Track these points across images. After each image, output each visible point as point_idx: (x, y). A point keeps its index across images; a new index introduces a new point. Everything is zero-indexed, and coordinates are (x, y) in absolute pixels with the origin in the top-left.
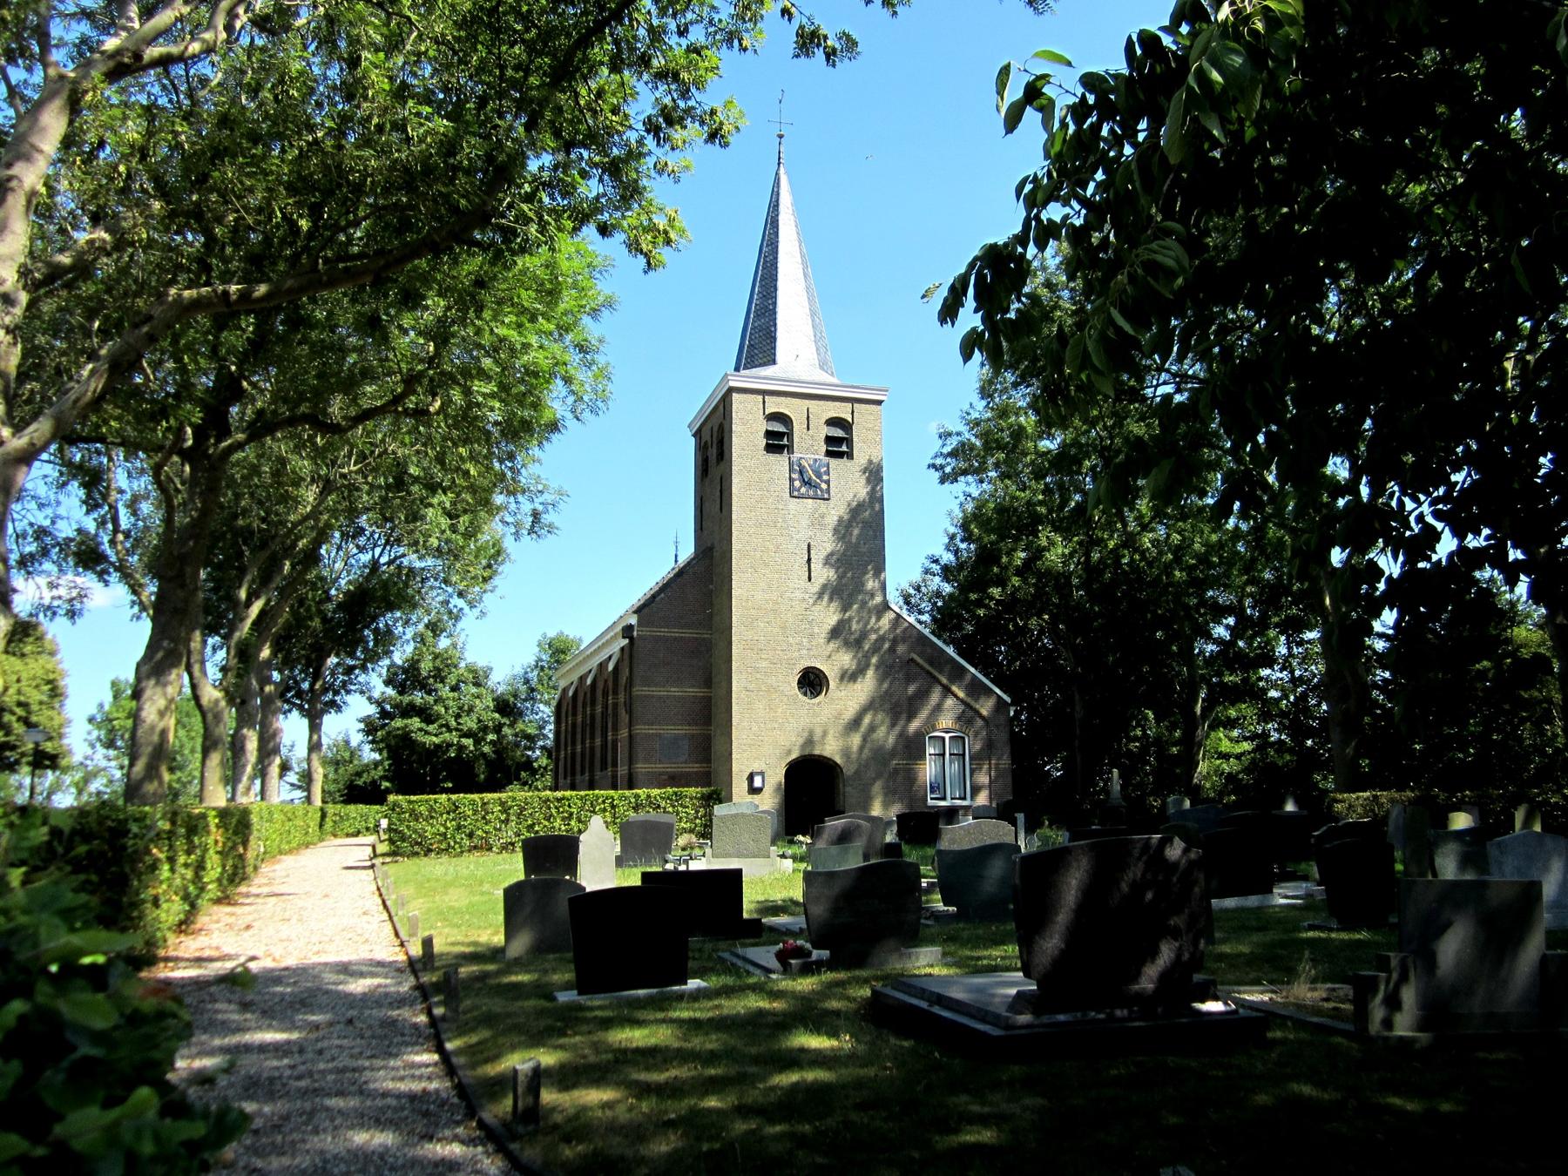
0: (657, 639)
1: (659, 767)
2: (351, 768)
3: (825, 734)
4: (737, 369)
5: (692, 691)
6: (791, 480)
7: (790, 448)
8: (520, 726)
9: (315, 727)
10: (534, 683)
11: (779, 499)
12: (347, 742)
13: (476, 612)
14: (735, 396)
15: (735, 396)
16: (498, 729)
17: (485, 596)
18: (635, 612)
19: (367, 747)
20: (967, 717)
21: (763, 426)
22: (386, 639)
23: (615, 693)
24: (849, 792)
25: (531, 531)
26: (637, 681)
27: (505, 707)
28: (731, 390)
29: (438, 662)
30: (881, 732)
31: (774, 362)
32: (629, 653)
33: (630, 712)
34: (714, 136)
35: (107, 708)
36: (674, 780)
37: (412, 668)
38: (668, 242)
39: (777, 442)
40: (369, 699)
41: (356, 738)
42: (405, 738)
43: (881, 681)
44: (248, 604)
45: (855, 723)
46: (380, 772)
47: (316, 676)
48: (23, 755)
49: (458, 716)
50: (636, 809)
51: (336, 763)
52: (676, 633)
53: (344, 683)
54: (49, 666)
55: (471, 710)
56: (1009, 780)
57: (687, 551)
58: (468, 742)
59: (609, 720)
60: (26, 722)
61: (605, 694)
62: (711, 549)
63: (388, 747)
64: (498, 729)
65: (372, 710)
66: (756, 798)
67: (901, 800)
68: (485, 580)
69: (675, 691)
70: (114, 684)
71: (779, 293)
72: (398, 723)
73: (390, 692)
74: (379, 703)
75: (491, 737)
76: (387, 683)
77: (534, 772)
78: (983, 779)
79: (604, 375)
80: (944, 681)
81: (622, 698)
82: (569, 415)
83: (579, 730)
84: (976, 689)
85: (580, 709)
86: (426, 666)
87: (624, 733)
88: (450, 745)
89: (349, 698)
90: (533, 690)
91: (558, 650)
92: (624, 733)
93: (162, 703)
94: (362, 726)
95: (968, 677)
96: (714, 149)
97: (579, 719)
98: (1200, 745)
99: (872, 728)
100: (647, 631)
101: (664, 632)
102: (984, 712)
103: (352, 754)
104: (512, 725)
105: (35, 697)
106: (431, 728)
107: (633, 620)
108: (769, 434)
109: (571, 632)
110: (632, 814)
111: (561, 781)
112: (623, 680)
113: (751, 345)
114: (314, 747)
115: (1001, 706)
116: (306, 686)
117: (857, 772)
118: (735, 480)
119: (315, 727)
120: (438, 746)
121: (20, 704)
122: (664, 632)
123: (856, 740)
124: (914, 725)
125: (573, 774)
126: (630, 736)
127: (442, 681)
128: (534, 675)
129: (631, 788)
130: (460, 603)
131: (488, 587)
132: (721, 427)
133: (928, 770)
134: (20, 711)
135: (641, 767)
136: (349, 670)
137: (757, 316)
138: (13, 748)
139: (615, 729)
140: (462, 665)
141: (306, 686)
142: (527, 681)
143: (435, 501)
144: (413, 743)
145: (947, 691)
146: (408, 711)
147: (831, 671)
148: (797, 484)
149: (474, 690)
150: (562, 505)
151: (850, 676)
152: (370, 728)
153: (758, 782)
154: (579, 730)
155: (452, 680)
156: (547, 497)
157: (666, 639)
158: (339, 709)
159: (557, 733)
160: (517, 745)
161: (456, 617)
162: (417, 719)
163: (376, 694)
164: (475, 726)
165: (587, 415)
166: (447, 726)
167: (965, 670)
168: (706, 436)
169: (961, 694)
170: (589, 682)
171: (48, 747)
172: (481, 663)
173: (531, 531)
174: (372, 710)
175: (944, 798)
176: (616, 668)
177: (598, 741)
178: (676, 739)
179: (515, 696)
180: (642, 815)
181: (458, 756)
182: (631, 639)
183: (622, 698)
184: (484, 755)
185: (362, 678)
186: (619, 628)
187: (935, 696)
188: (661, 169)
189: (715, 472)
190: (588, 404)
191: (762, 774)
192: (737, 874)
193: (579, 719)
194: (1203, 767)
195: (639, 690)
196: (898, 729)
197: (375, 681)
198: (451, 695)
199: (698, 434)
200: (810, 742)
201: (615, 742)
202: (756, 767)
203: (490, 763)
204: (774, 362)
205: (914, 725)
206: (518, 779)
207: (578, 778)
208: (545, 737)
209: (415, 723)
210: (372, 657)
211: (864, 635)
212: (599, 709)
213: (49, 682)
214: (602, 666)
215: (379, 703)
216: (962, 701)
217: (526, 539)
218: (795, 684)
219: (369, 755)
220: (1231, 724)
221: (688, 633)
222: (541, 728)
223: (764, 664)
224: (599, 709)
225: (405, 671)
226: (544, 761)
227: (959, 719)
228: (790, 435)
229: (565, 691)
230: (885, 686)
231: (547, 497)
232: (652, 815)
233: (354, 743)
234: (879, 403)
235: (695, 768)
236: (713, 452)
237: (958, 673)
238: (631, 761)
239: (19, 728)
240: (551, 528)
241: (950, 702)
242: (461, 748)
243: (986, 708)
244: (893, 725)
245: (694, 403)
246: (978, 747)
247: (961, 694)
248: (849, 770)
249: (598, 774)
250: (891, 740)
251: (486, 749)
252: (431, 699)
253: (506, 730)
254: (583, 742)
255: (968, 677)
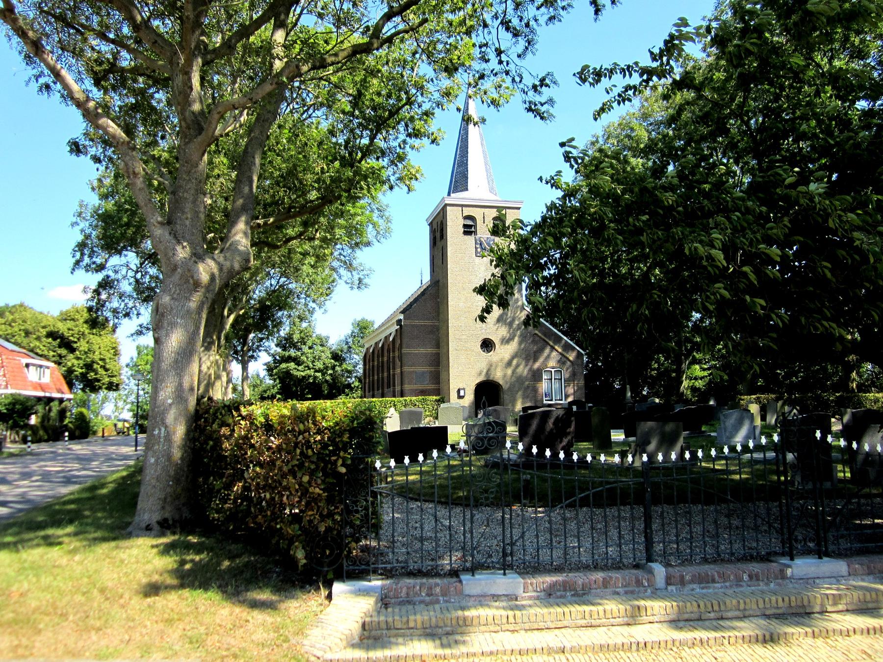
0: (413, 326)
1: (415, 387)
2: (261, 389)
3: (496, 366)
4: (449, 194)
5: (430, 350)
6: (476, 248)
7: (475, 233)
8: (344, 366)
9: (245, 369)
10: (351, 344)
11: (471, 257)
12: (258, 375)
13: (322, 310)
14: (448, 208)
15: (448, 208)
16: (333, 368)
17: (327, 302)
18: (402, 312)
19: (267, 377)
20: (563, 360)
21: (462, 222)
22: (278, 324)
23: (394, 351)
24: (506, 397)
25: (359, 288)
26: (404, 346)
27: (336, 357)
28: (446, 205)
29: (302, 335)
30: (520, 369)
31: (467, 189)
32: (400, 332)
33: (401, 360)
34: (433, 142)
35: (135, 360)
36: (423, 392)
37: (289, 338)
38: (417, 179)
39: (469, 230)
40: (269, 354)
41: (263, 373)
42: (288, 373)
43: (520, 343)
44: (228, 316)
45: (509, 364)
46: (275, 390)
47: (245, 343)
48: (103, 384)
49: (313, 362)
50: (405, 406)
51: (255, 386)
52: (422, 323)
53: (258, 347)
54: (113, 340)
55: (319, 359)
56: (583, 391)
57: (427, 278)
58: (319, 375)
59: (391, 364)
60: (104, 367)
61: (389, 351)
62: (438, 281)
63: (279, 377)
64: (333, 368)
65: (269, 359)
66: (461, 401)
67: (531, 401)
68: (327, 295)
69: (422, 350)
70: (138, 347)
71: (469, 155)
72: (284, 365)
73: (279, 350)
74: (273, 356)
75: (330, 372)
76: (277, 345)
77: (351, 389)
78: (571, 390)
79: (388, 220)
80: (551, 343)
81: (397, 354)
82: (375, 240)
83: (376, 369)
84: (567, 347)
85: (376, 359)
86: (296, 337)
87: (398, 371)
88: (309, 376)
89: (260, 354)
90: (350, 347)
91: (362, 328)
92: (398, 371)
93: (209, 364)
94: (265, 367)
95: (563, 342)
96: (434, 146)
97: (376, 363)
98: (684, 372)
99: (517, 366)
100: (408, 322)
101: (417, 322)
102: (571, 358)
103: (261, 381)
104: (340, 366)
105: (108, 355)
106: (300, 368)
107: (401, 317)
108: (465, 226)
109: (369, 318)
110: (403, 408)
111: (367, 394)
112: (397, 345)
113: (456, 181)
114: (245, 378)
115: (579, 355)
116: (239, 348)
117: (509, 388)
118: (449, 249)
119: (245, 369)
120: (304, 377)
121: (101, 359)
122: (417, 322)
123: (509, 372)
124: (537, 365)
125: (373, 390)
126: (401, 372)
127: (305, 344)
128: (350, 340)
129: (402, 396)
130: (314, 305)
131: (328, 298)
132: (442, 223)
133: (544, 386)
134: (101, 363)
135: (407, 387)
136: (261, 339)
137: (459, 166)
138: (99, 381)
139: (394, 368)
140: (314, 335)
141: (239, 348)
142: (347, 343)
143: (306, 262)
144: (292, 375)
145: (553, 348)
146: (289, 359)
147: (496, 340)
148: (479, 250)
149: (321, 348)
150: (371, 276)
151: (506, 341)
152: (270, 370)
153: (462, 393)
154: (376, 369)
155: (309, 343)
156: (365, 272)
157: (417, 326)
158: (256, 359)
159: (365, 370)
160: (343, 376)
161: (312, 312)
162: (293, 364)
163: (272, 352)
164: (322, 367)
165: (382, 240)
166: (308, 367)
167: (562, 338)
168: (435, 226)
169: (560, 350)
170: (380, 345)
171: (115, 380)
172: (324, 334)
173: (359, 288)
174: (269, 359)
175: (552, 400)
176: (394, 339)
177: (385, 374)
178: (423, 373)
179: (342, 351)
180: (408, 409)
181: (314, 381)
182: (401, 326)
183: (397, 354)
184: (327, 381)
185: (267, 344)
186: (394, 321)
187: (547, 351)
188: (412, 148)
189: (439, 243)
190: (383, 234)
191: (464, 389)
192: (445, 429)
193: (376, 363)
194: (685, 383)
195: (404, 351)
196: (528, 367)
197: (272, 345)
198: (309, 351)
199: (431, 224)
200: (488, 373)
201: (394, 375)
202: (461, 386)
203: (329, 385)
204: (467, 189)
205: (537, 365)
206: (344, 392)
207: (376, 392)
208: (358, 372)
209: (292, 365)
210: (271, 334)
211: (513, 320)
212: (385, 359)
213: (114, 348)
214: (386, 338)
215: (273, 356)
216: (561, 354)
217: (356, 290)
218: (479, 347)
219: (269, 382)
220: (699, 362)
221: (428, 323)
222: (355, 367)
223: (464, 337)
224: (385, 359)
225: (286, 339)
226: (357, 384)
227: (559, 361)
228: (475, 226)
229: (368, 349)
230: (523, 346)
231: (365, 272)
232: (413, 409)
233: (262, 376)
234: (519, 208)
235: (432, 387)
236: (438, 235)
237: (558, 340)
238: (402, 384)
239: (101, 371)
240: (366, 286)
241: (554, 353)
242: (315, 378)
243: (572, 356)
244: (527, 365)
245: (429, 209)
246: (567, 376)
247: (560, 350)
248: (505, 387)
249: (386, 390)
250: (526, 372)
251: (328, 378)
252: (299, 353)
253: (337, 368)
254: (378, 375)
255: (563, 342)
